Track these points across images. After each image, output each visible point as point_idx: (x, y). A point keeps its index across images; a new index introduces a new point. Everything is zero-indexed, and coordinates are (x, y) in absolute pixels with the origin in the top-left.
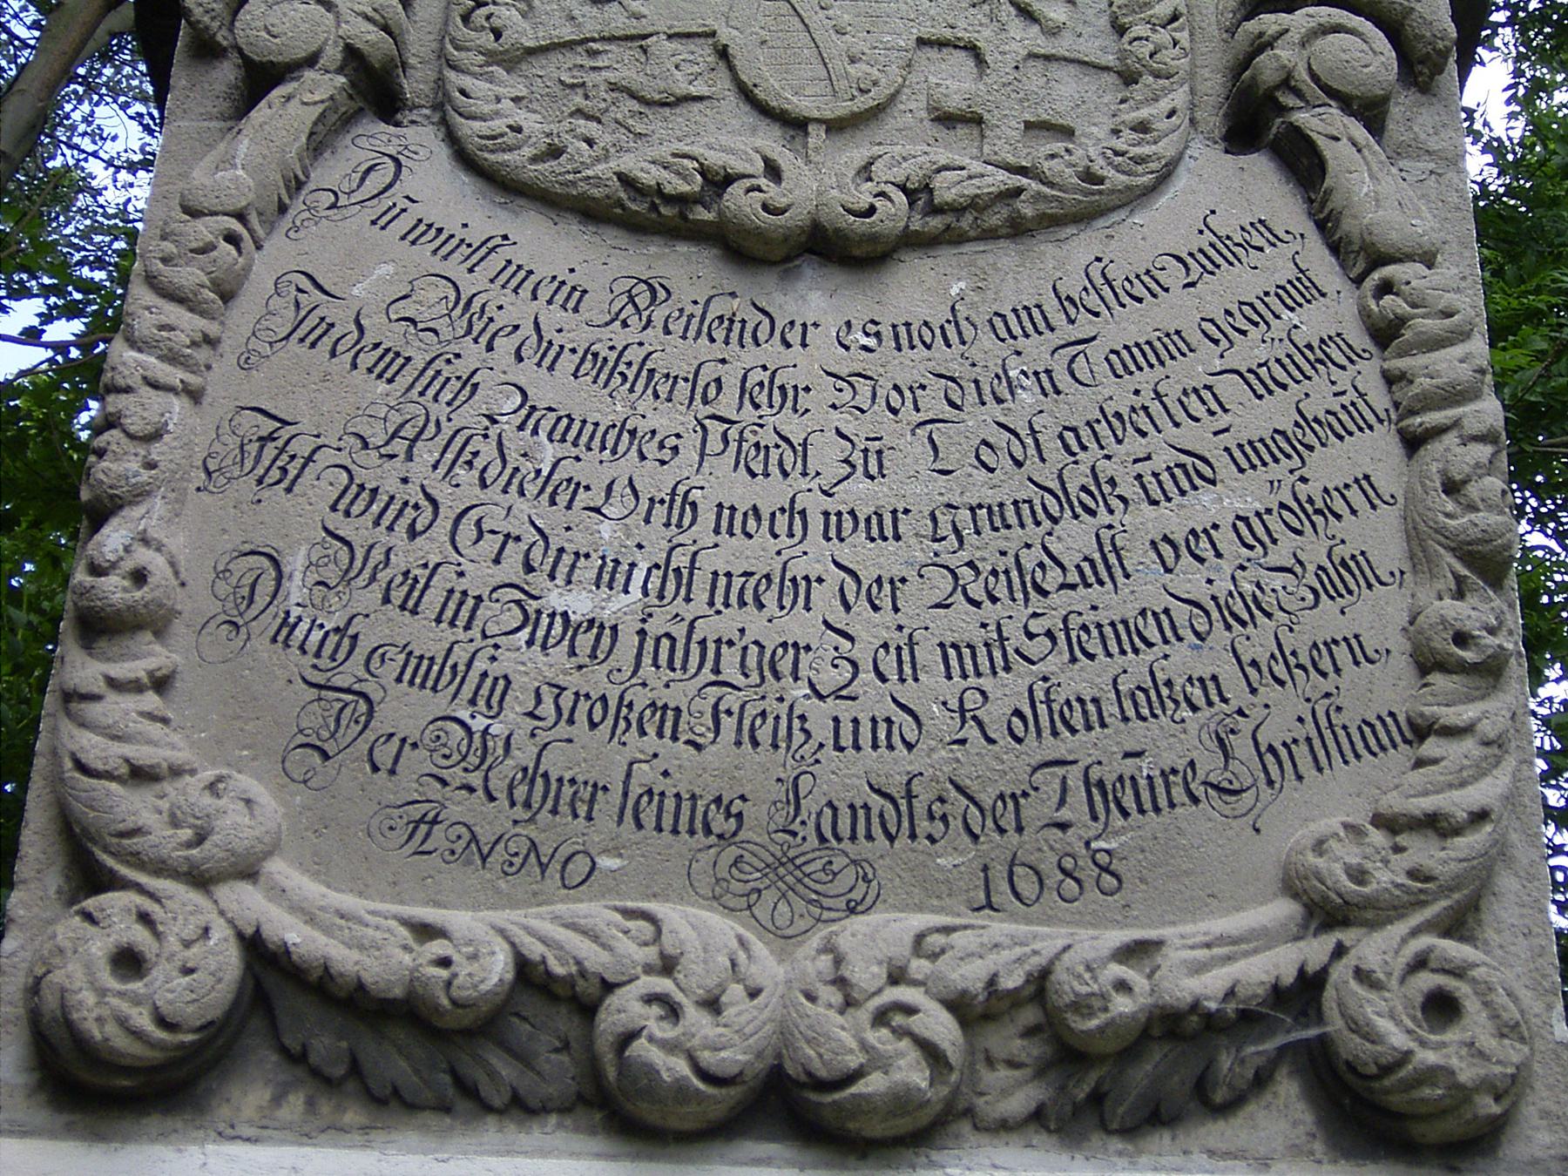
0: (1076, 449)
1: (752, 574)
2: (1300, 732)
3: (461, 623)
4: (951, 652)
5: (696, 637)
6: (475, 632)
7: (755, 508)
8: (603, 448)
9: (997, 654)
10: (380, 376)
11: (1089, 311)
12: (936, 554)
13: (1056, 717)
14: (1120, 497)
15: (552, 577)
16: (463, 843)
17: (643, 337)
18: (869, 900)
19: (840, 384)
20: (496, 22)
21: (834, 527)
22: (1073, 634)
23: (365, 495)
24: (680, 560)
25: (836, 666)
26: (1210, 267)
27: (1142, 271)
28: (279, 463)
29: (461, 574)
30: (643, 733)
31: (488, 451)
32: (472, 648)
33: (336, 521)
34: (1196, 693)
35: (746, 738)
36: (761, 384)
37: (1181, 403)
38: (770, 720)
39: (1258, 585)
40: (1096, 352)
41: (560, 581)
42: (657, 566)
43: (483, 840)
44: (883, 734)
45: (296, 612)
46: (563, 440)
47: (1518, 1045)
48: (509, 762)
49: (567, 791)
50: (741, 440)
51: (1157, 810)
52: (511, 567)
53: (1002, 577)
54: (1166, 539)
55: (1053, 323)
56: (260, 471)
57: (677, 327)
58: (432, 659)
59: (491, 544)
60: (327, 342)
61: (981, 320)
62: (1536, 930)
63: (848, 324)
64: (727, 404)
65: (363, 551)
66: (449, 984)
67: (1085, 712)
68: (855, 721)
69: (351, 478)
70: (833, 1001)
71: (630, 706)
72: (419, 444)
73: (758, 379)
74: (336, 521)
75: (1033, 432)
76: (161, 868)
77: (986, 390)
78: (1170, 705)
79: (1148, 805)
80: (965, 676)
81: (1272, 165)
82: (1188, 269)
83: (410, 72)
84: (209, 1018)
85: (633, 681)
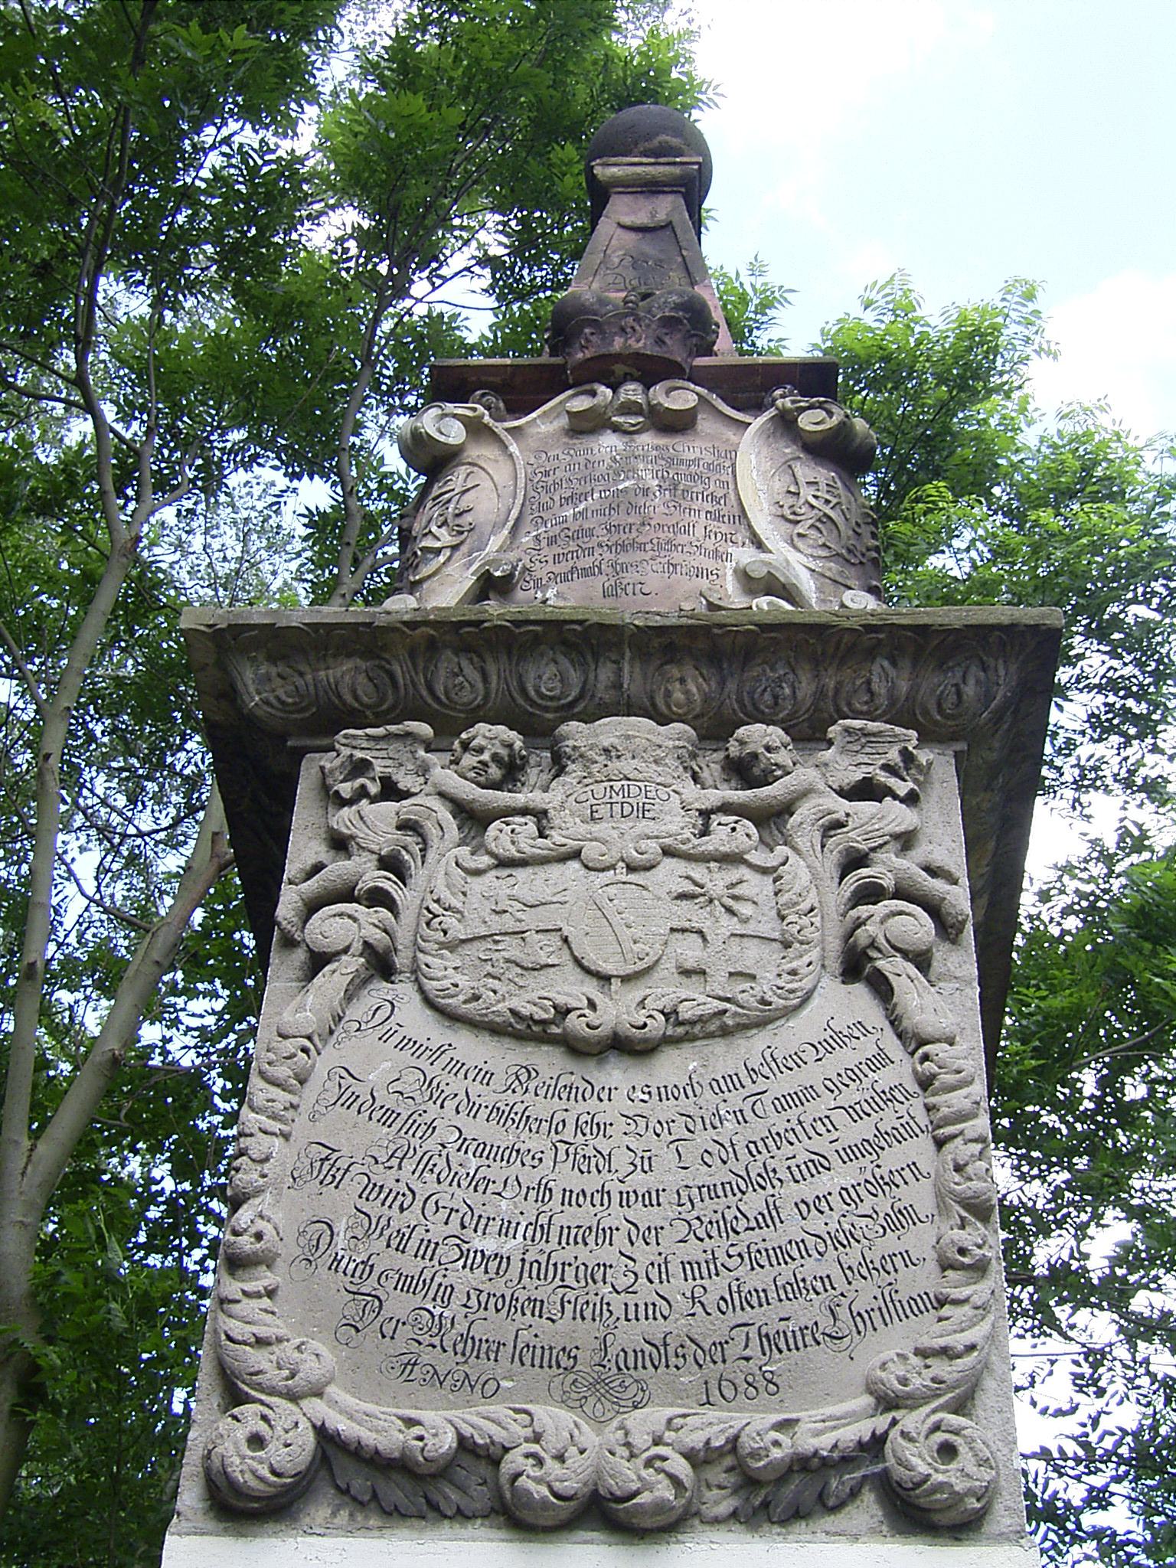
0: (755, 1153)
3: (427, 1257)
4: (688, 1267)
5: (552, 1262)
6: (435, 1262)
9: (712, 1267)
15: (475, 1231)
24: (543, 1220)
30: (524, 1314)
31: (441, 1163)
33: (362, 1204)
40: (767, 1099)
44: (651, 1311)
49: (484, 1346)
51: (798, 1349)
52: (454, 1227)
54: (803, 1201)
56: (321, 1177)
57: (542, 1092)
59: (443, 1214)
66: (423, 1450)
74: (362, 1204)
77: (708, 1122)
78: (804, 1292)
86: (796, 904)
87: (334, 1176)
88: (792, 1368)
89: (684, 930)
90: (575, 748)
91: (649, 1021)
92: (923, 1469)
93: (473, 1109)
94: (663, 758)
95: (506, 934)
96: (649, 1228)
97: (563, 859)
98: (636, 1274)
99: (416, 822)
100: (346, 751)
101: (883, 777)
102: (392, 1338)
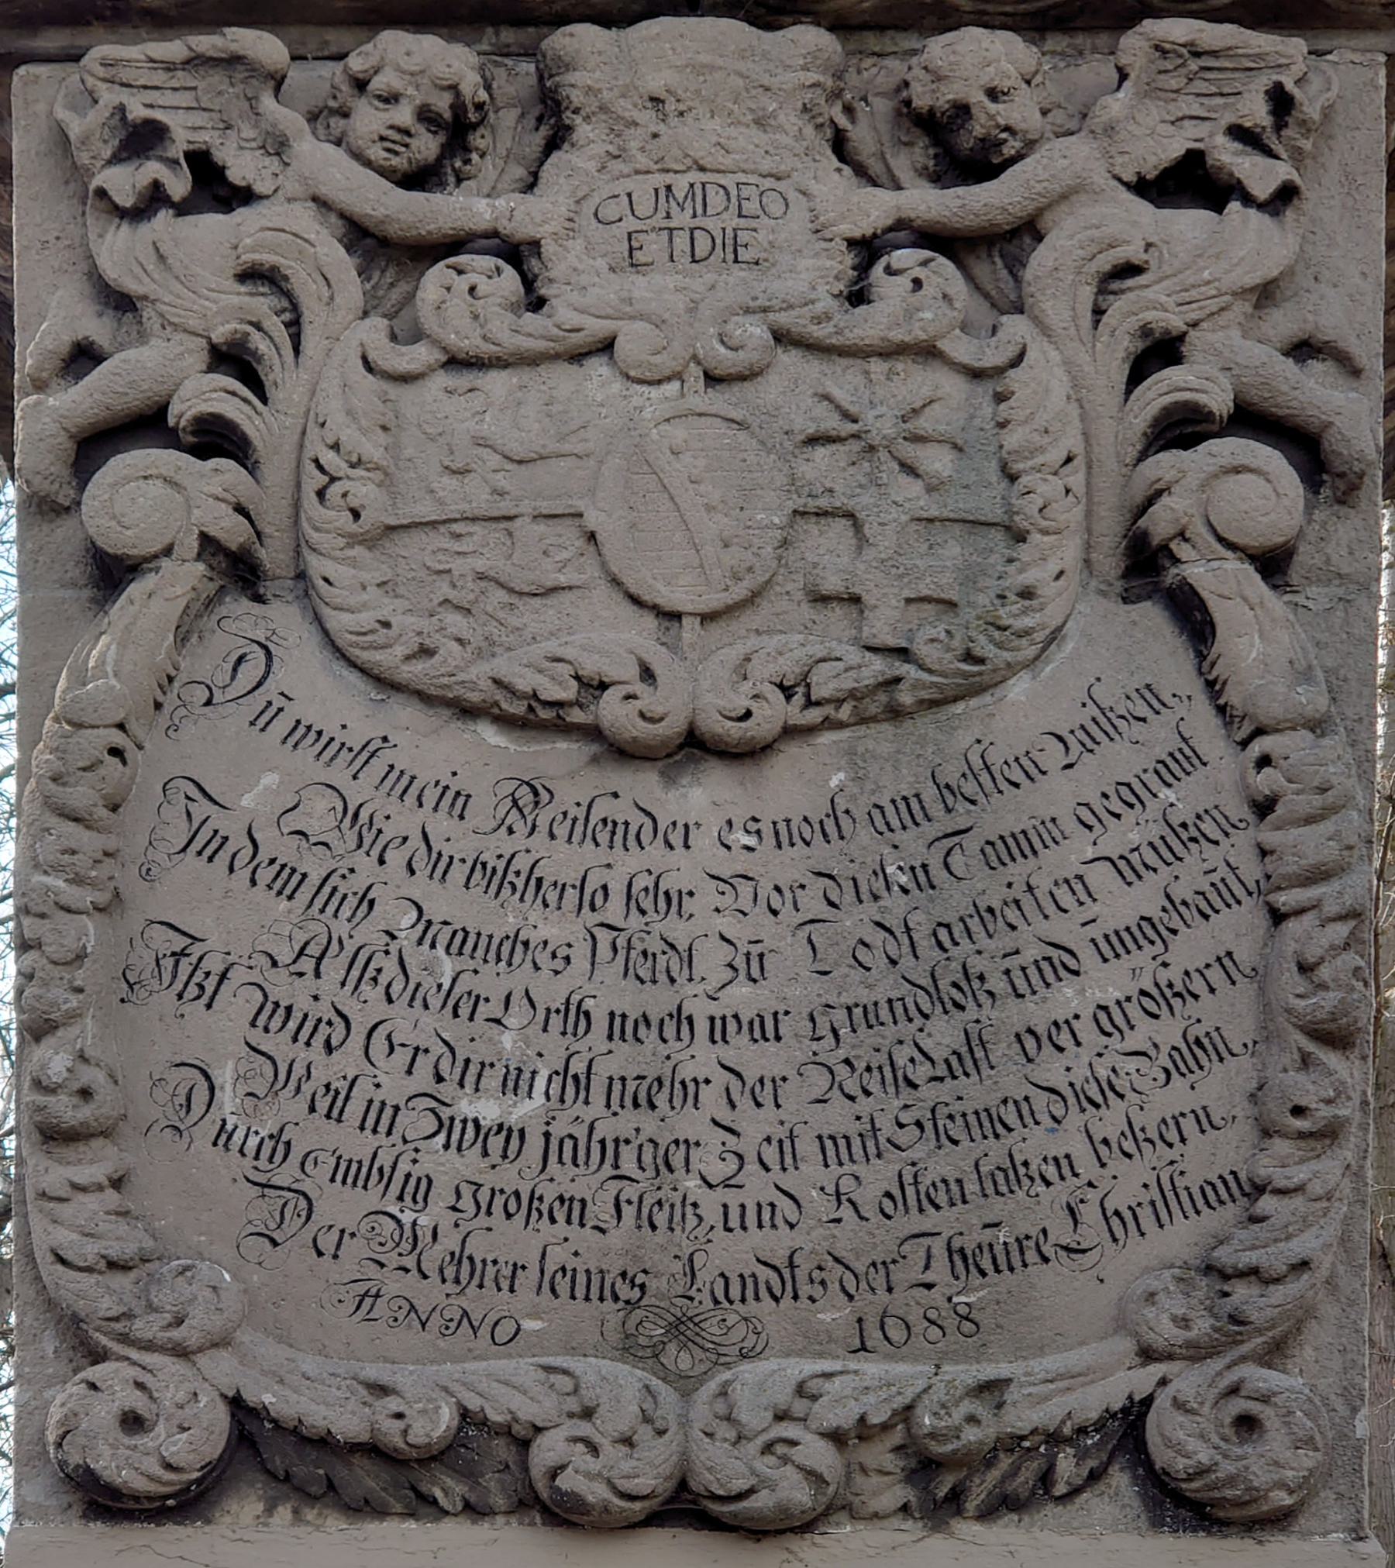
0: (947, 943)
1: (644, 1078)
2: (1145, 1197)
3: (383, 1128)
4: (829, 1143)
5: (596, 1137)
6: (396, 1137)
7: (644, 1016)
8: (499, 960)
9: (870, 1144)
10: (280, 893)
11: (966, 799)
12: (815, 1054)
13: (923, 1197)
14: (990, 993)
15: (461, 1085)
16: (404, 1312)
17: (531, 843)
18: (758, 1349)
19: (723, 887)
20: (354, 503)
21: (718, 1031)
22: (940, 1123)
23: (281, 1011)
24: (578, 1066)
25: (724, 1160)
26: (1090, 744)
27: (1021, 753)
28: (196, 979)
29: (378, 1086)
30: (553, 1220)
31: (391, 967)
32: (395, 1152)
33: (256, 1037)
34: (1051, 1171)
35: (646, 1223)
36: (646, 889)
37: (1052, 895)
38: (667, 1207)
39: (1114, 1070)
40: (972, 843)
41: (469, 1088)
42: (557, 1073)
43: (420, 1310)
44: (766, 1216)
45: (231, 1122)
46: (460, 954)
47: (1311, 1453)
48: (437, 1247)
49: (491, 1270)
50: (629, 948)
51: (1011, 1269)
52: (423, 1077)
53: (876, 1073)
54: (1030, 1031)
55: (931, 813)
56: (178, 986)
57: (561, 831)
58: (360, 1162)
59: (402, 1057)
60: (224, 857)
61: (859, 813)
62: (1349, 1347)
63: (730, 823)
64: (614, 910)
65: (286, 1066)
66: (405, 1432)
67: (948, 1191)
68: (743, 1206)
69: (266, 996)
70: (727, 1436)
71: (541, 1199)
72: (325, 961)
73: (643, 885)
74: (256, 1037)
75: (908, 929)
76: (149, 1346)
77: (864, 888)
78: (1026, 1181)
79: (1003, 1266)
80: (841, 1164)
81: (1167, 614)
82: (1067, 749)
83: (267, 541)
84: (207, 1460)
85: (542, 1177)
86: (1041, 450)
87: (201, 987)
88: (1003, 1297)
89: (822, 514)
90: (589, 90)
91: (754, 706)
92: (1204, 1456)
93: (441, 866)
94: (773, 115)
95: (474, 519)
96: (761, 1081)
97: (577, 357)
98: (740, 1157)
99: (274, 269)
100: (110, 97)
101: (1229, 157)
102: (335, 1257)
